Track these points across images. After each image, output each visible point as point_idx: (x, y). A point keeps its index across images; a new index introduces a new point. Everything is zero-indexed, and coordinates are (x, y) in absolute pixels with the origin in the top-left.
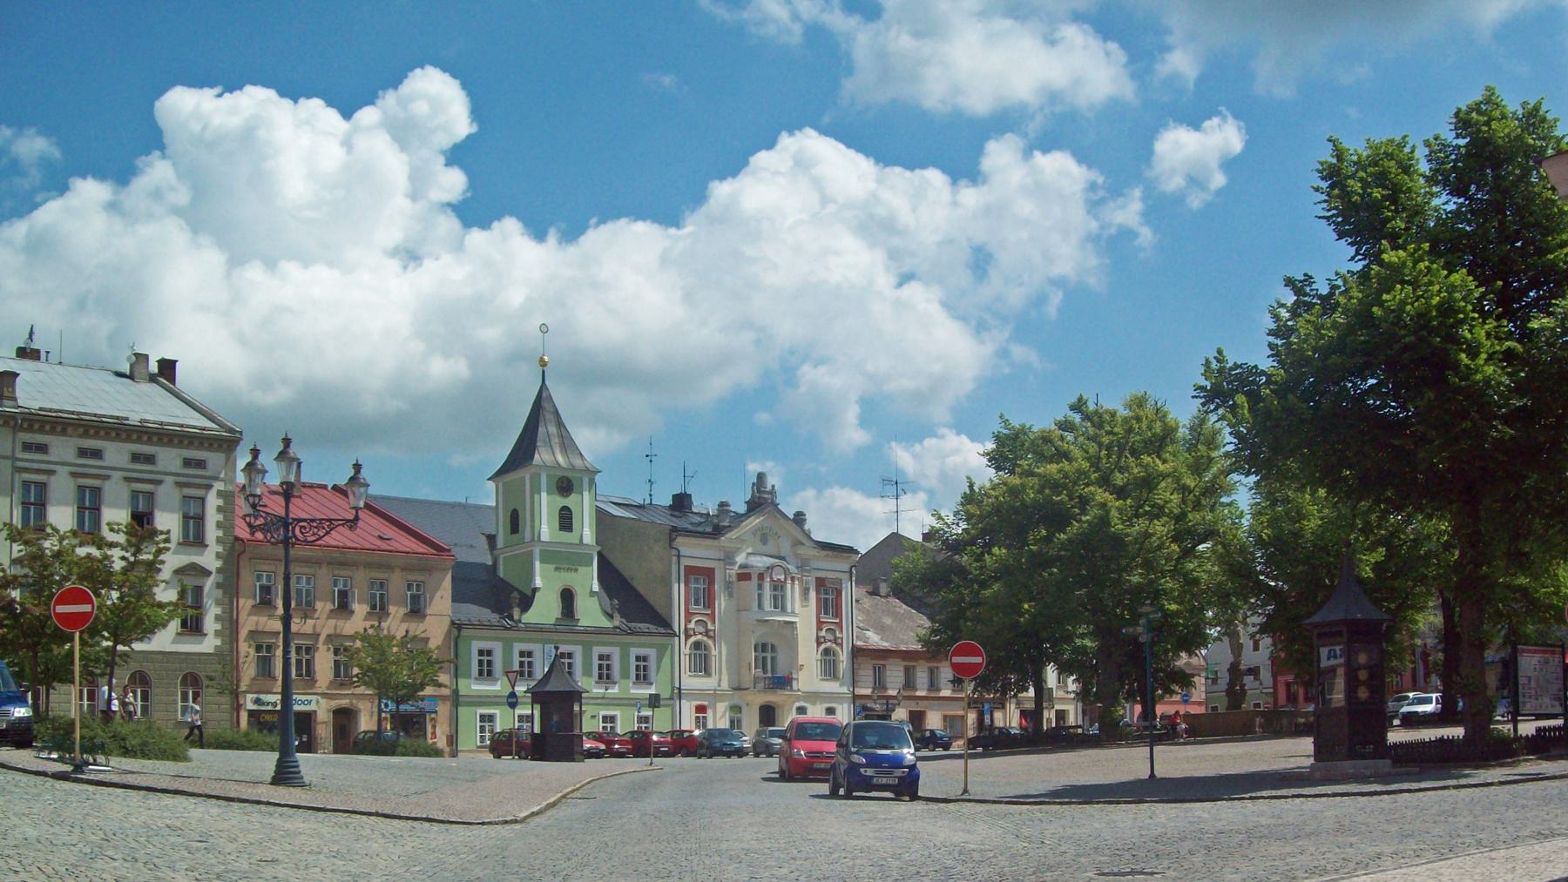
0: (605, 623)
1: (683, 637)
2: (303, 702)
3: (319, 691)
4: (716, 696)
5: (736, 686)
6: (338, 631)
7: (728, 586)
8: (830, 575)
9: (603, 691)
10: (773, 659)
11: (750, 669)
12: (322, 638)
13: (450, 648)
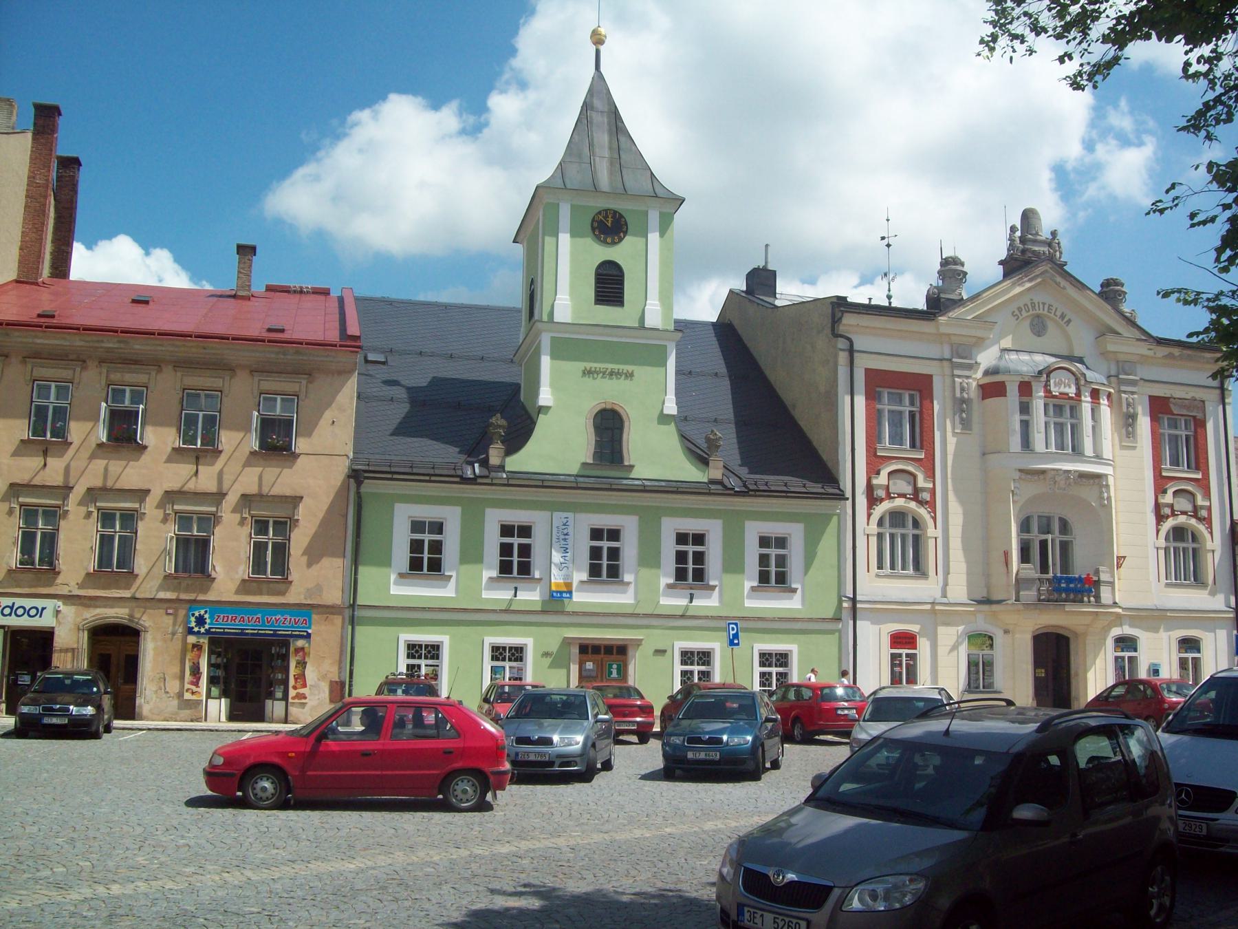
0: (691, 473)
1: (862, 501)
2: (27, 612)
3: (64, 591)
4: (937, 614)
5: (981, 593)
6: (109, 484)
7: (961, 405)
8: (1178, 393)
9: (684, 602)
10: (1065, 548)
11: (1007, 563)
12: (232, 499)
13: (346, 516)
